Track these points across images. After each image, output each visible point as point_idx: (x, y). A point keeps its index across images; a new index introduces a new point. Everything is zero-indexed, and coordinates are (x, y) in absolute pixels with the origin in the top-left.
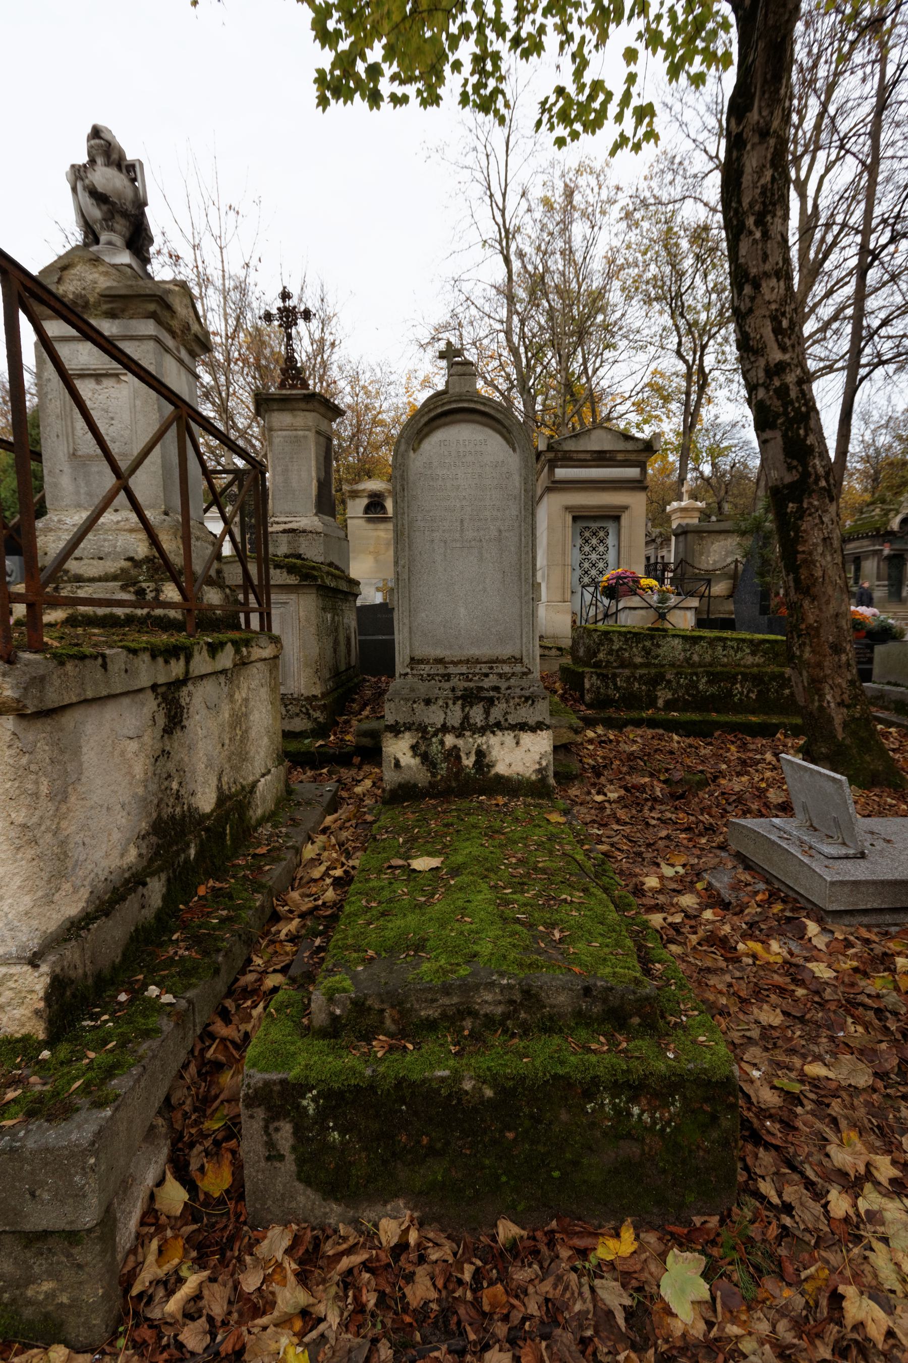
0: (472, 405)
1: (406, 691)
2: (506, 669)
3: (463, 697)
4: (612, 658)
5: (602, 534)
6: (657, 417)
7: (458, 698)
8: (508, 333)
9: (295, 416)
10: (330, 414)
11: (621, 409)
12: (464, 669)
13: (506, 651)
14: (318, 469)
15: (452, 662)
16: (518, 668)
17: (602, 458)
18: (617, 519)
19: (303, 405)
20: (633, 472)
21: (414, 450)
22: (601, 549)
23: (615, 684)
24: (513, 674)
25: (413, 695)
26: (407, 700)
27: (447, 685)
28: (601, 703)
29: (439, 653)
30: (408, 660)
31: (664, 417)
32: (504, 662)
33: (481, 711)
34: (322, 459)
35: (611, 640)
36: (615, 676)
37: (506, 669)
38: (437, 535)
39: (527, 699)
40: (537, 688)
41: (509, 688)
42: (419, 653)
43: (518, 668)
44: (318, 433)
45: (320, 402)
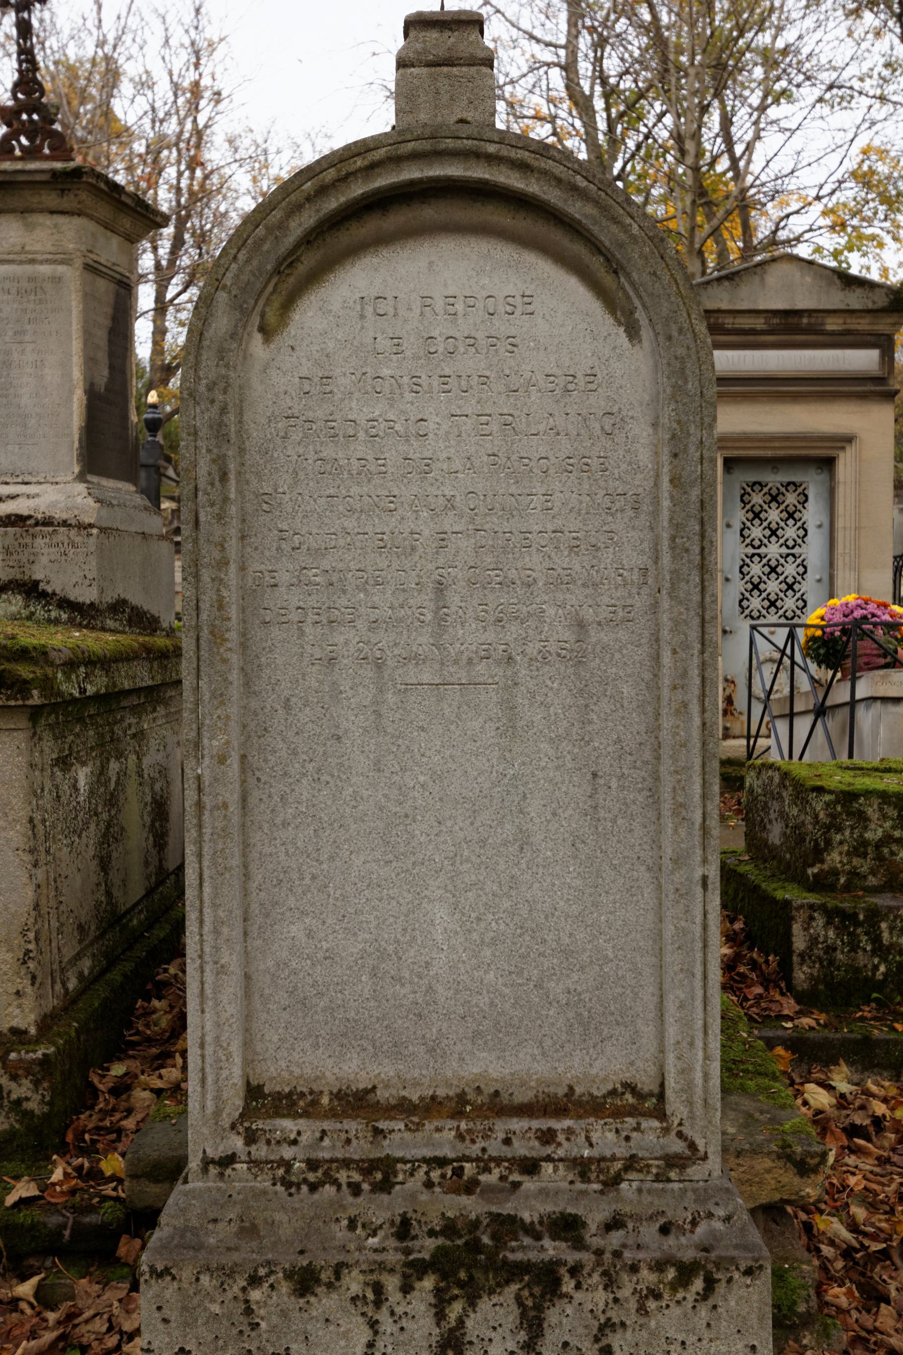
0: (479, 172)
1: (225, 1231)
2: (605, 1139)
3: (441, 1265)
4: (864, 865)
5: (791, 499)
6: (873, 237)
7: (419, 1269)
8: (569, 68)
9: (30, 227)
10: (126, 223)
11: (797, 224)
12: (441, 1138)
13: (600, 1067)
14: (89, 361)
15: (402, 1107)
16: (650, 1138)
17: (791, 328)
18: (827, 464)
19: (50, 199)
20: (864, 360)
21: (267, 332)
22: (791, 532)
23: (876, 939)
24: (632, 1163)
25: (247, 1254)
26: (228, 1273)
27: (380, 1210)
28: (837, 992)
29: (354, 1069)
30: (235, 1102)
31: (888, 239)
32: (594, 1107)
33: (509, 1316)
34: (101, 336)
35: (862, 818)
36: (874, 915)
37: (605, 1139)
38: (346, 639)
39: (686, 1273)
40: (727, 1224)
41: (614, 1224)
42: (279, 1071)
43: (650, 1138)
44: (92, 269)
45: (94, 189)
